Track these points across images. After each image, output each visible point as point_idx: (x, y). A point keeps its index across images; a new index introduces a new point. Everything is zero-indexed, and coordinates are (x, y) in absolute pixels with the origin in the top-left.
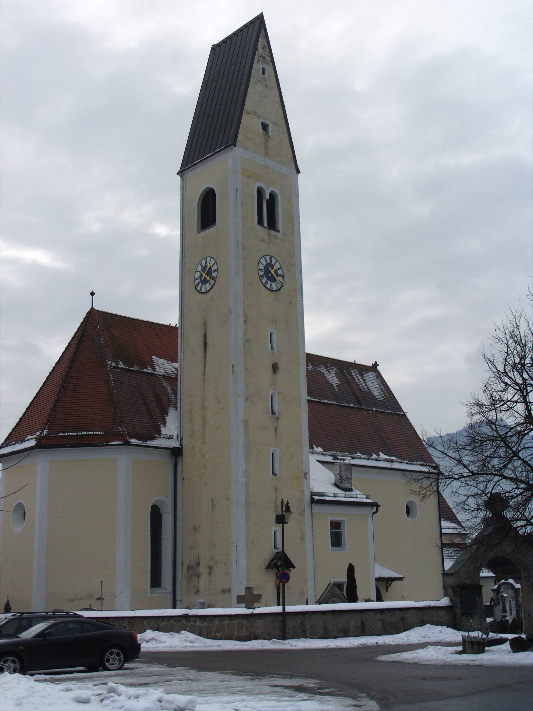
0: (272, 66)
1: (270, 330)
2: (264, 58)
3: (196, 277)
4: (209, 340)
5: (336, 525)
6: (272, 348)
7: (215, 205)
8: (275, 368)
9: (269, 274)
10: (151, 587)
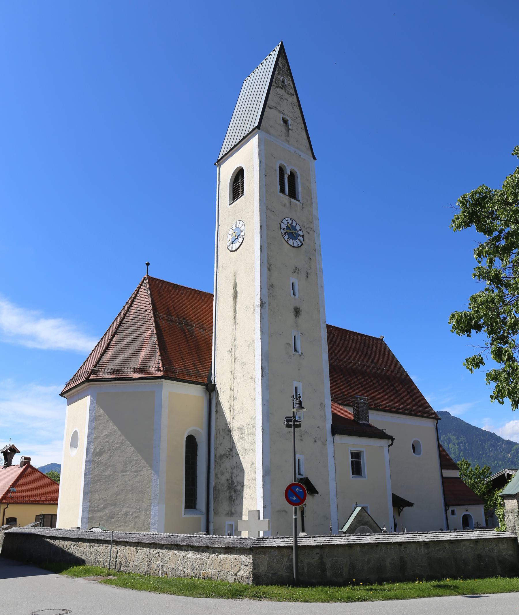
5: (356, 455)
6: (294, 294)
8: (297, 312)
9: (291, 233)
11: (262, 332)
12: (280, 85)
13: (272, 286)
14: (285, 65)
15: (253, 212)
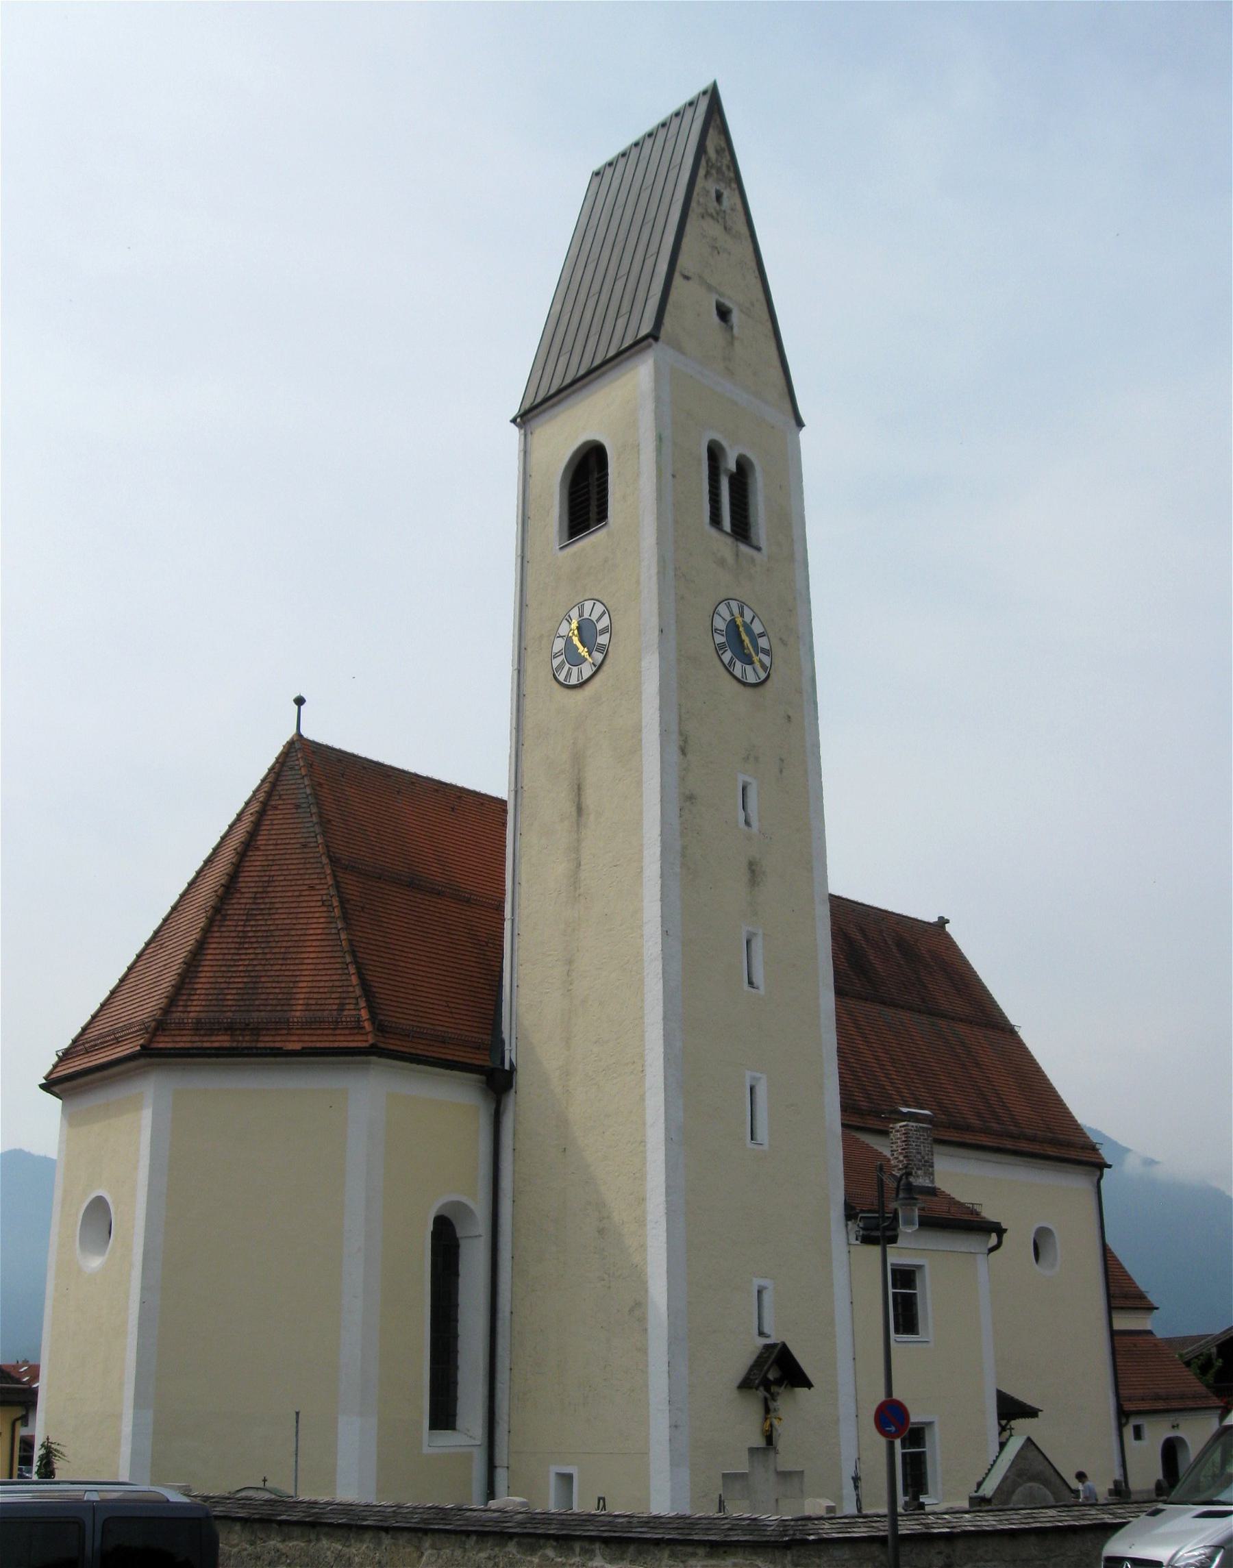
0: (737, 192)
1: (742, 778)
2: (719, 170)
3: (556, 650)
4: (590, 799)
6: (747, 823)
7: (606, 495)
8: (754, 871)
9: (737, 642)
10: (431, 1428)
11: (665, 933)
12: (712, 211)
13: (690, 798)
14: (723, 150)
15: (638, 582)
